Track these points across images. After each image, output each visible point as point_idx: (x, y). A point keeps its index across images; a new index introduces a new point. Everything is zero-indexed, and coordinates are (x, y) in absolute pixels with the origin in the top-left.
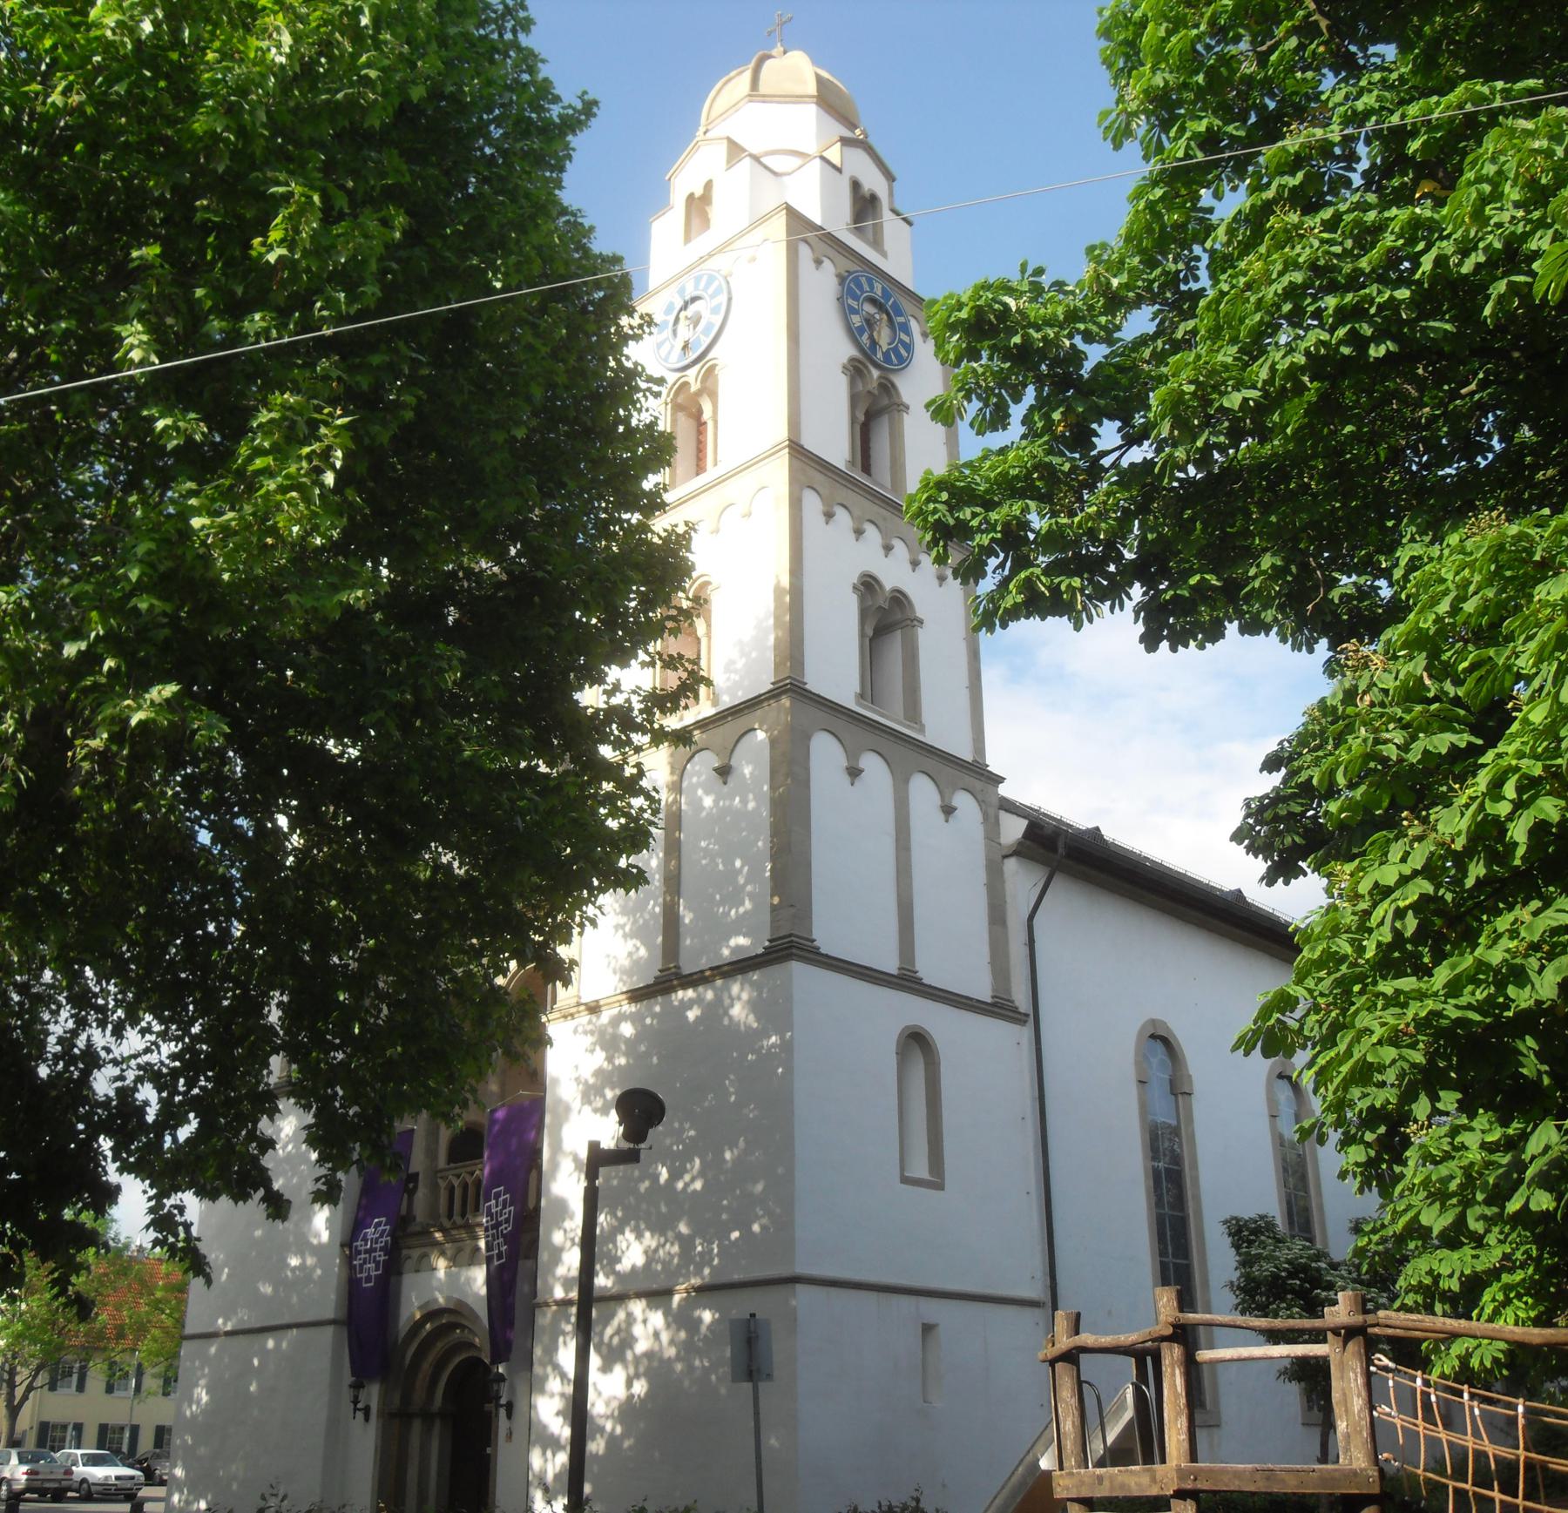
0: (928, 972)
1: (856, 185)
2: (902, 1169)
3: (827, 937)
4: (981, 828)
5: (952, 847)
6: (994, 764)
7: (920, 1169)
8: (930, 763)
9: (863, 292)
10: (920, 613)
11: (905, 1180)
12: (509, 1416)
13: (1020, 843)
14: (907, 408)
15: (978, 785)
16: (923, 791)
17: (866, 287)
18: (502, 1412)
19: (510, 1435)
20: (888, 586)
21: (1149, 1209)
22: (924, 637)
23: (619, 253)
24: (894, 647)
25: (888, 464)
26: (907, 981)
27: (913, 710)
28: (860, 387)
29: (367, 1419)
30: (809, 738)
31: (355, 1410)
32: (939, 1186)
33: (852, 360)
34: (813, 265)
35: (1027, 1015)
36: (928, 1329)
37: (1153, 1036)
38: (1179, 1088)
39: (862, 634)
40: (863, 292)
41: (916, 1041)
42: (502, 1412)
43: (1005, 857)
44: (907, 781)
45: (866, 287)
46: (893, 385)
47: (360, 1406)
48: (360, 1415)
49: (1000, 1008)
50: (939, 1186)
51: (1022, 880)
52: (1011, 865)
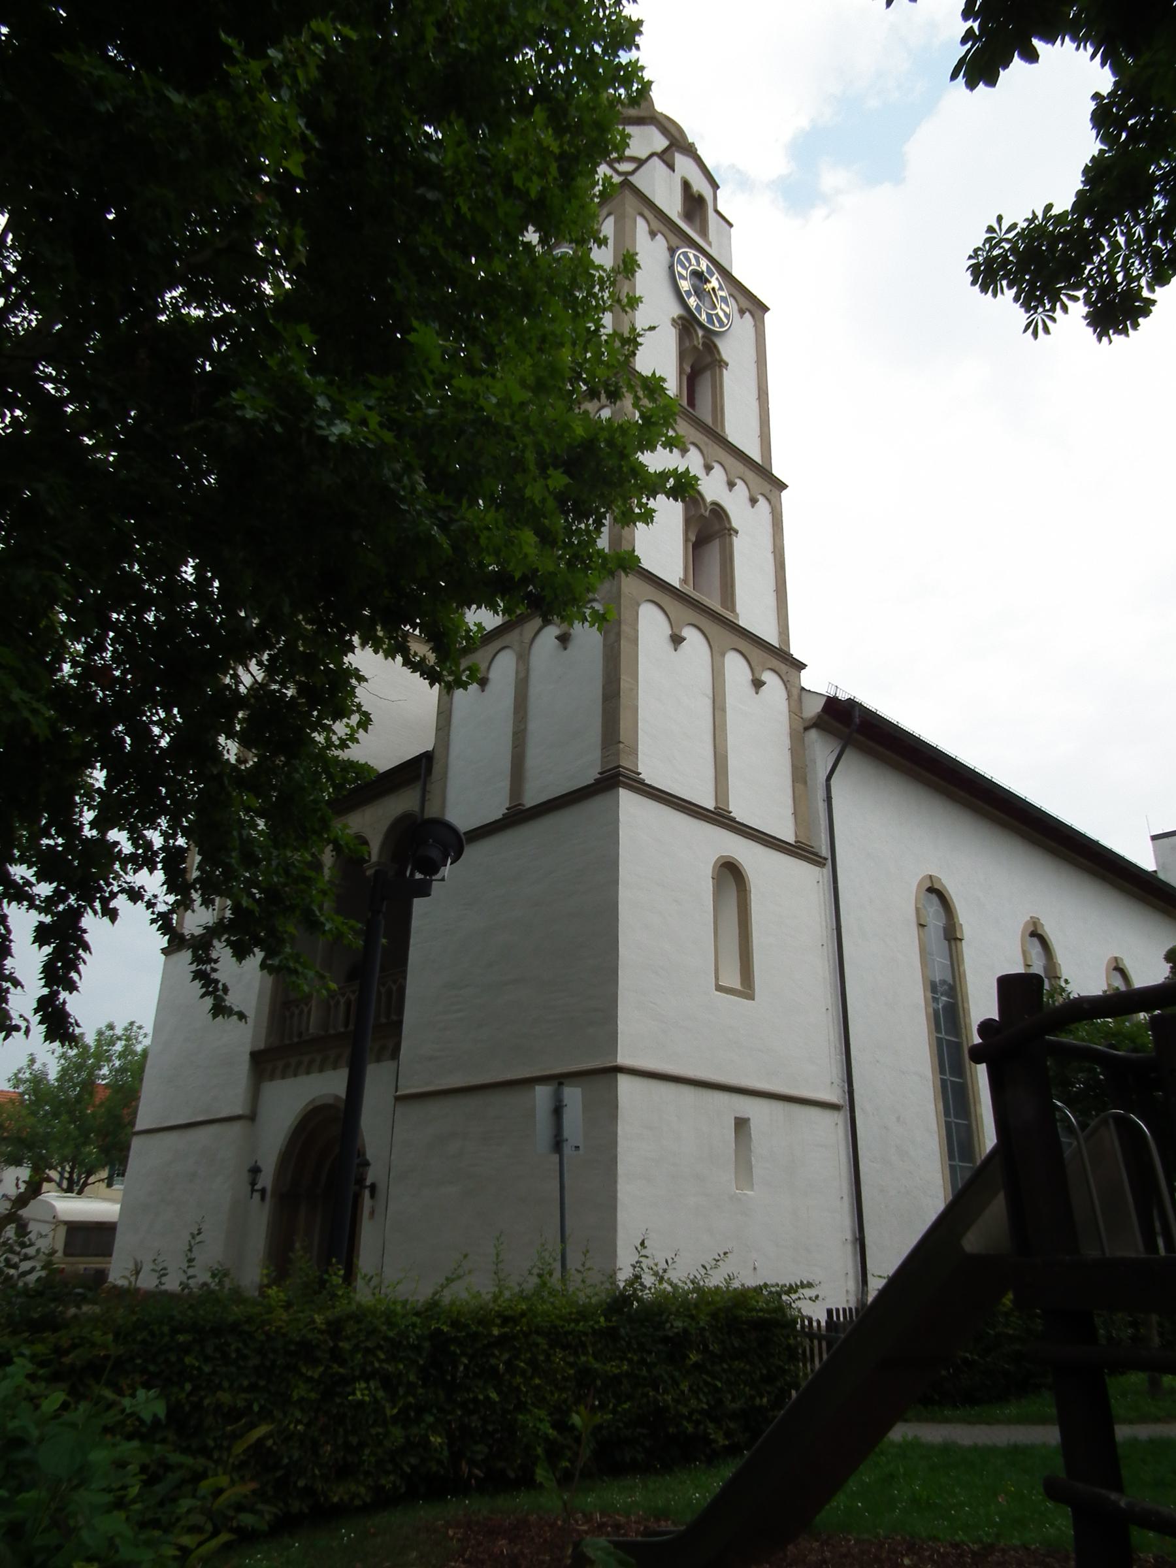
0: (739, 811)
1: (686, 185)
2: (717, 979)
3: (650, 769)
4: (786, 703)
5: (761, 723)
6: (797, 651)
7: (732, 979)
8: (744, 645)
9: (690, 265)
10: (735, 524)
11: (719, 988)
12: (372, 1196)
13: (819, 717)
14: (727, 365)
15: (783, 668)
16: (736, 668)
17: (693, 261)
18: (367, 1193)
19: (372, 1213)
20: (709, 499)
21: (929, 1033)
22: (740, 545)
23: (568, 651)
24: (713, 550)
25: (710, 408)
26: (720, 818)
27: (732, 607)
28: (687, 344)
29: (263, 1198)
30: (639, 605)
31: (253, 1191)
32: (751, 997)
33: (680, 317)
34: (648, 237)
35: (826, 859)
36: (741, 1124)
37: (931, 890)
38: (952, 935)
39: (686, 540)
40: (690, 265)
41: (730, 873)
42: (367, 1193)
43: (806, 729)
44: (723, 655)
45: (693, 261)
46: (715, 346)
47: (257, 1187)
48: (257, 1196)
49: (800, 850)
50: (751, 997)
51: (822, 751)
52: (813, 734)
